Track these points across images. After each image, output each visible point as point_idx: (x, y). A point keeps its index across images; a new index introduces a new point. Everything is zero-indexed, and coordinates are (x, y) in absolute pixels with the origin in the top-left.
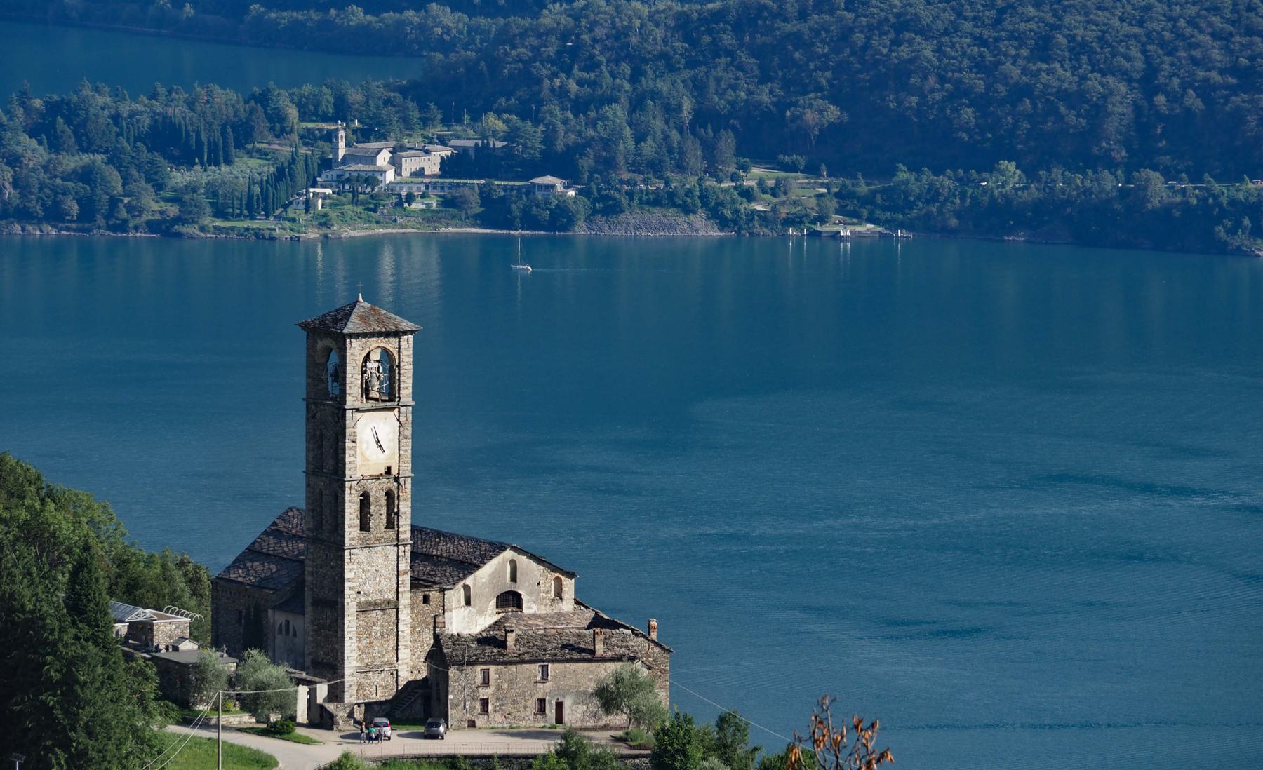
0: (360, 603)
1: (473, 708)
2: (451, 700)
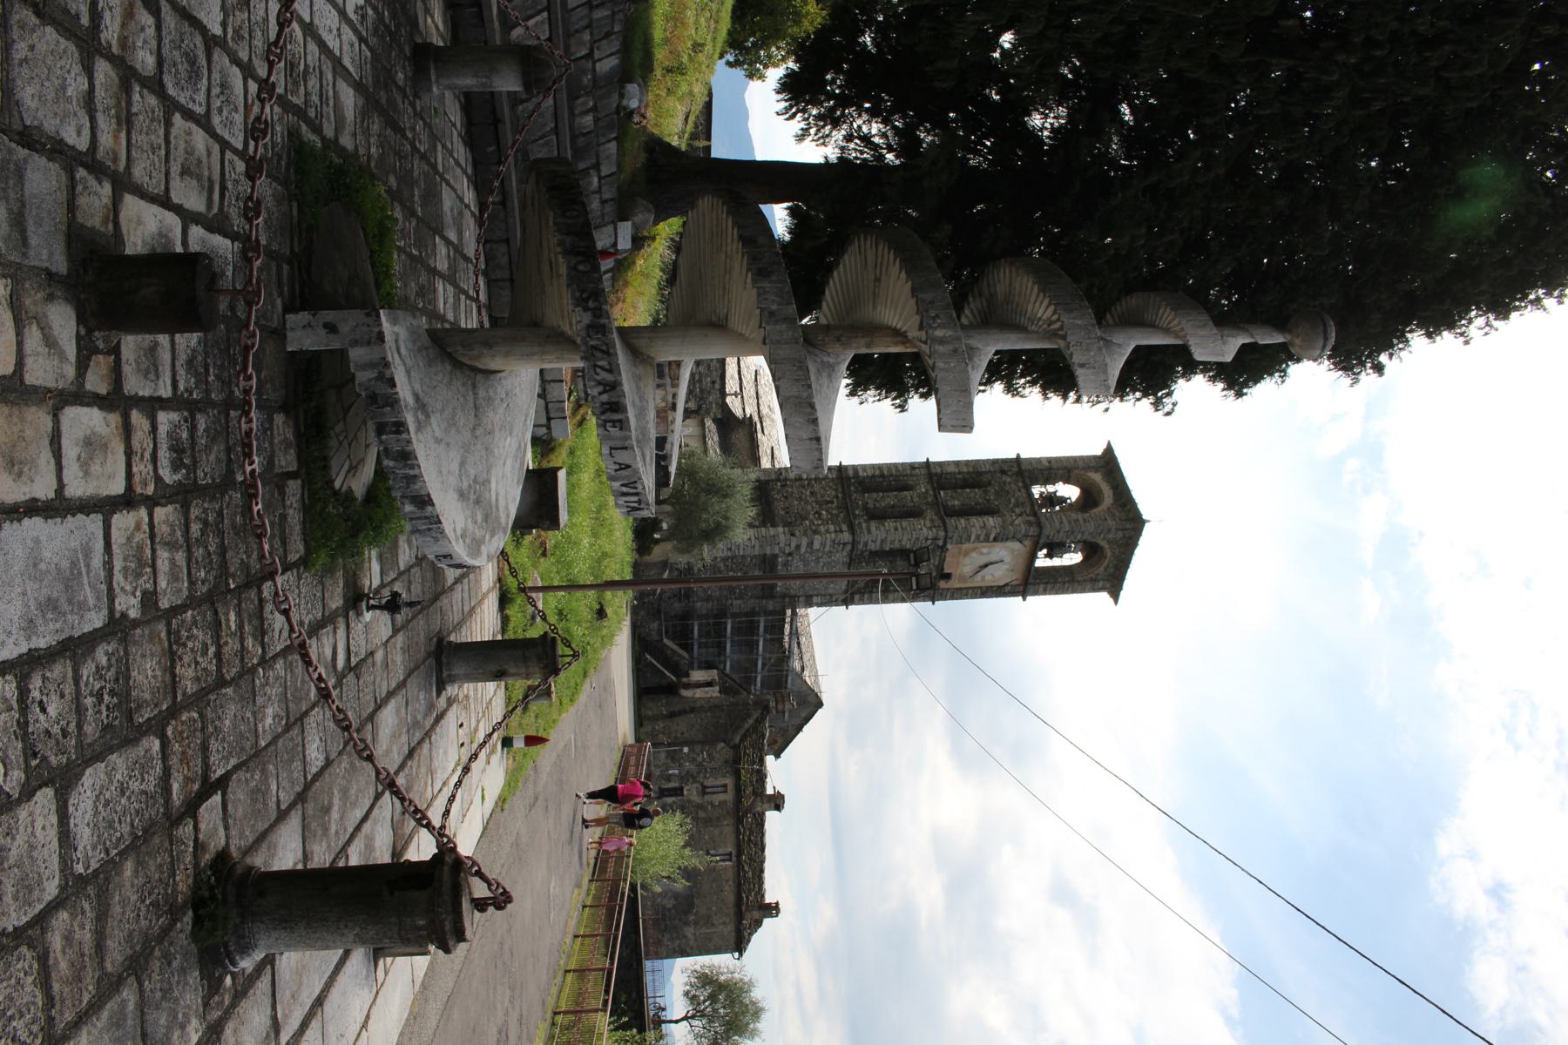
0: (776, 556)
1: (669, 778)
2: (681, 750)
